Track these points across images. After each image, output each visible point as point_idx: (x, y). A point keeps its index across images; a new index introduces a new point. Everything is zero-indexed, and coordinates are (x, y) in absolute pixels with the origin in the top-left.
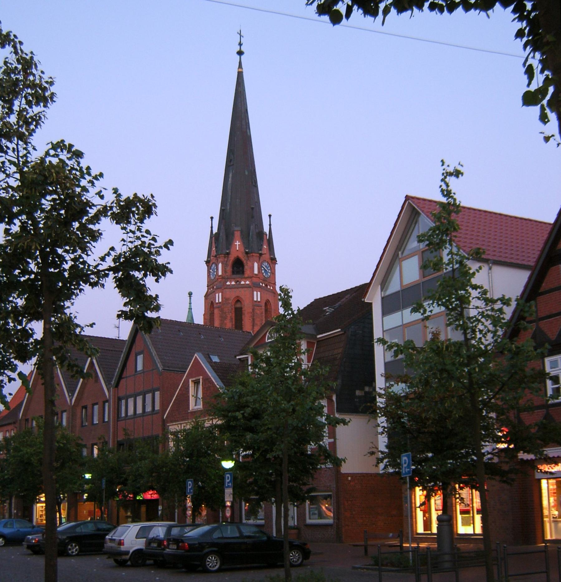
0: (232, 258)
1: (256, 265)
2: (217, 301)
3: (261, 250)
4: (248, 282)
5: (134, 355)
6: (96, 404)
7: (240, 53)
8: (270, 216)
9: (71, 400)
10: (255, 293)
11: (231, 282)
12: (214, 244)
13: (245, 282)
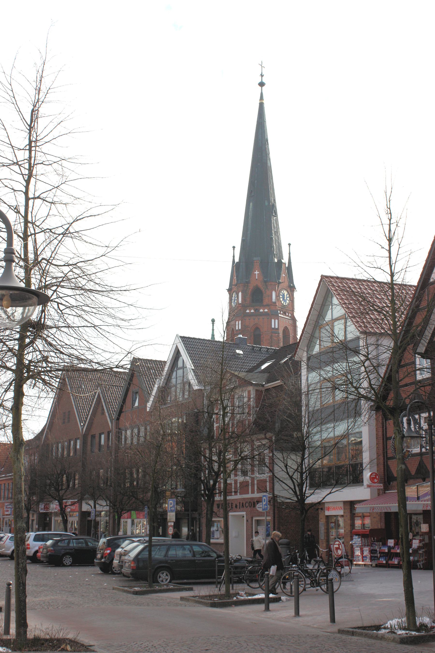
0: (251, 287)
1: (274, 294)
2: (237, 329)
3: (279, 279)
4: (266, 310)
5: (132, 392)
6: (103, 433)
7: (262, 84)
8: (289, 245)
9: (82, 429)
10: (273, 320)
11: (250, 310)
12: (235, 272)
13: (264, 310)
